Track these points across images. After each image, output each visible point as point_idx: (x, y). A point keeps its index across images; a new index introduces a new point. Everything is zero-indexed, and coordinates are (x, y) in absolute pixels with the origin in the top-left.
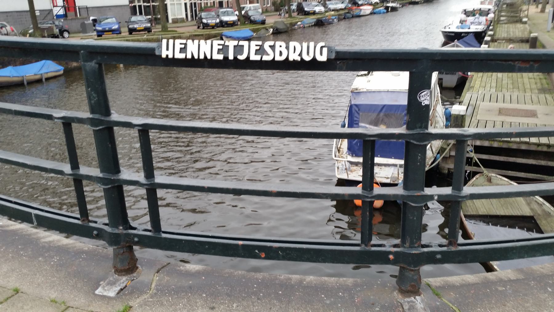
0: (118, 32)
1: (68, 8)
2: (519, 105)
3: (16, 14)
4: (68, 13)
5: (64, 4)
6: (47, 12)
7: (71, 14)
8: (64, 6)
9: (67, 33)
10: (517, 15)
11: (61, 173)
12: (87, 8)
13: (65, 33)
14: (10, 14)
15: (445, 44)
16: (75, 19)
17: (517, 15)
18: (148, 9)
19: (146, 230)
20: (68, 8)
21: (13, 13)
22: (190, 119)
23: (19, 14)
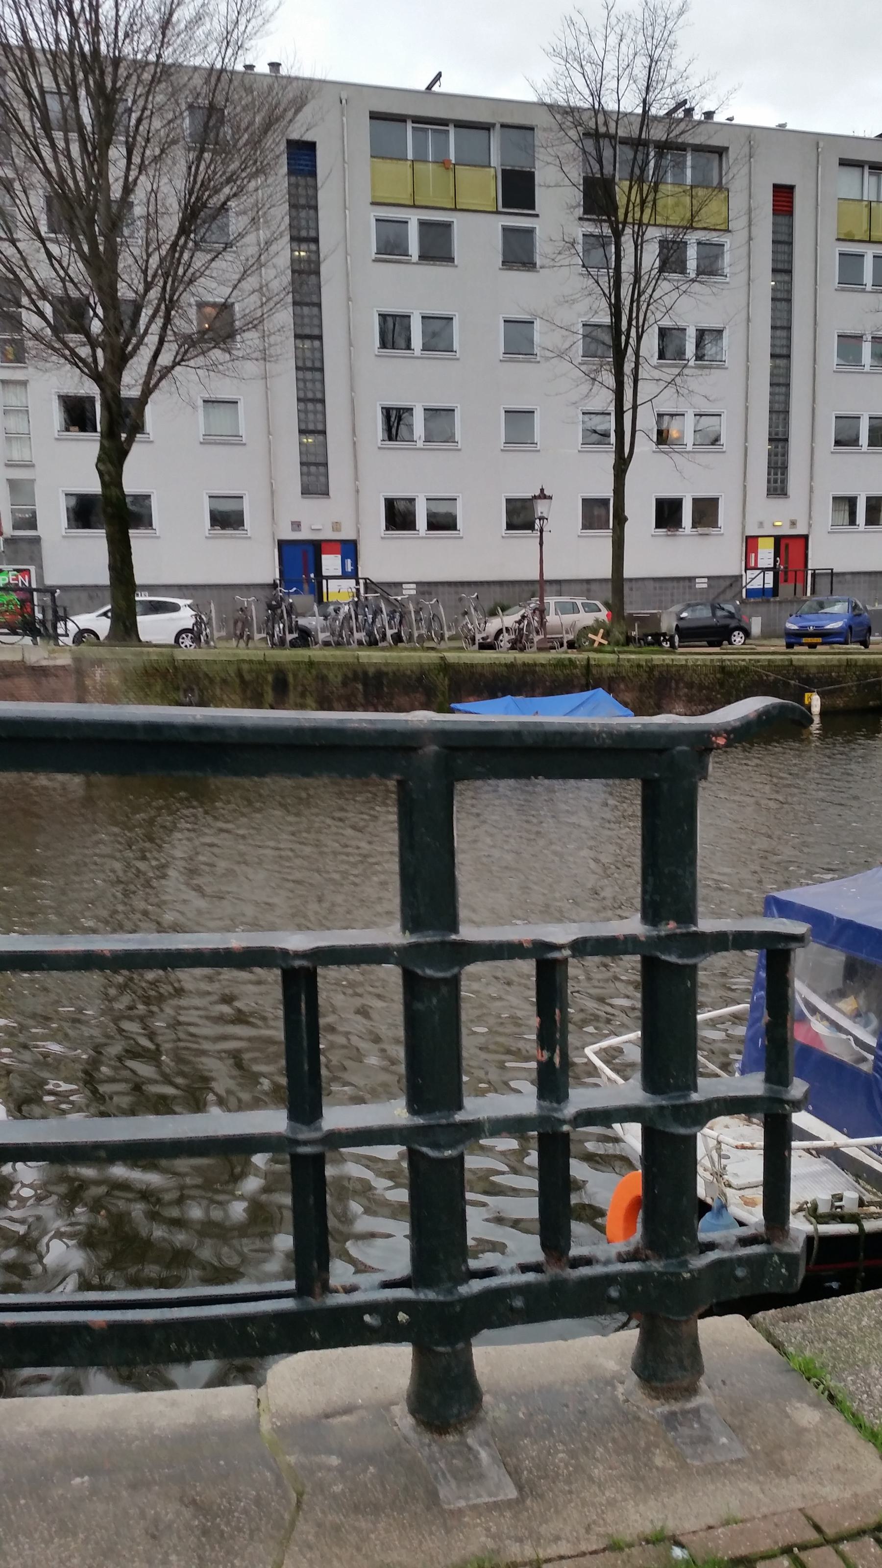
0: (841, 639)
1: (786, 573)
2: (502, 324)
3: (651, 584)
4: (782, 586)
5: (775, 561)
6: (728, 583)
7: (786, 589)
8: (774, 569)
9: (741, 634)
10: (411, 607)
11: (709, 886)
12: (832, 574)
13: (736, 633)
14: (640, 583)
15: (95, 431)
16: (791, 602)
17: (411, 607)
18: (596, 511)
19: (524, 1268)
20: (786, 573)
21: (646, 582)
22: (336, 1421)
23: (658, 585)
